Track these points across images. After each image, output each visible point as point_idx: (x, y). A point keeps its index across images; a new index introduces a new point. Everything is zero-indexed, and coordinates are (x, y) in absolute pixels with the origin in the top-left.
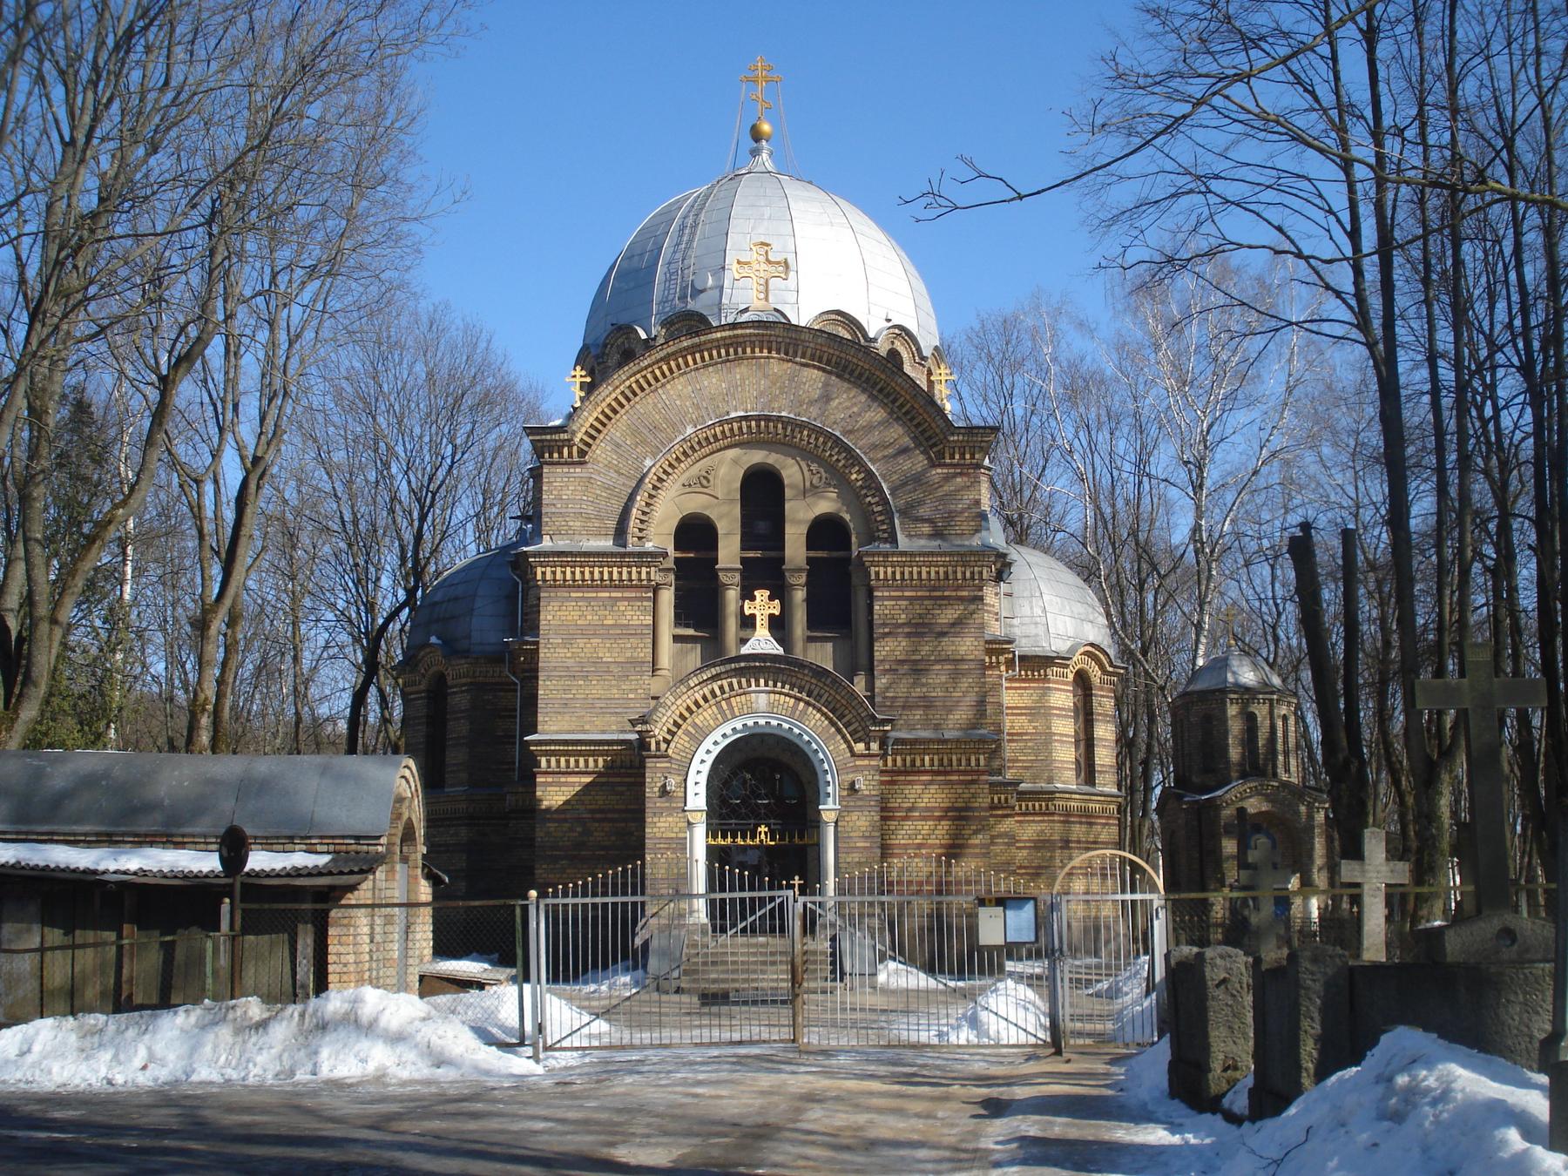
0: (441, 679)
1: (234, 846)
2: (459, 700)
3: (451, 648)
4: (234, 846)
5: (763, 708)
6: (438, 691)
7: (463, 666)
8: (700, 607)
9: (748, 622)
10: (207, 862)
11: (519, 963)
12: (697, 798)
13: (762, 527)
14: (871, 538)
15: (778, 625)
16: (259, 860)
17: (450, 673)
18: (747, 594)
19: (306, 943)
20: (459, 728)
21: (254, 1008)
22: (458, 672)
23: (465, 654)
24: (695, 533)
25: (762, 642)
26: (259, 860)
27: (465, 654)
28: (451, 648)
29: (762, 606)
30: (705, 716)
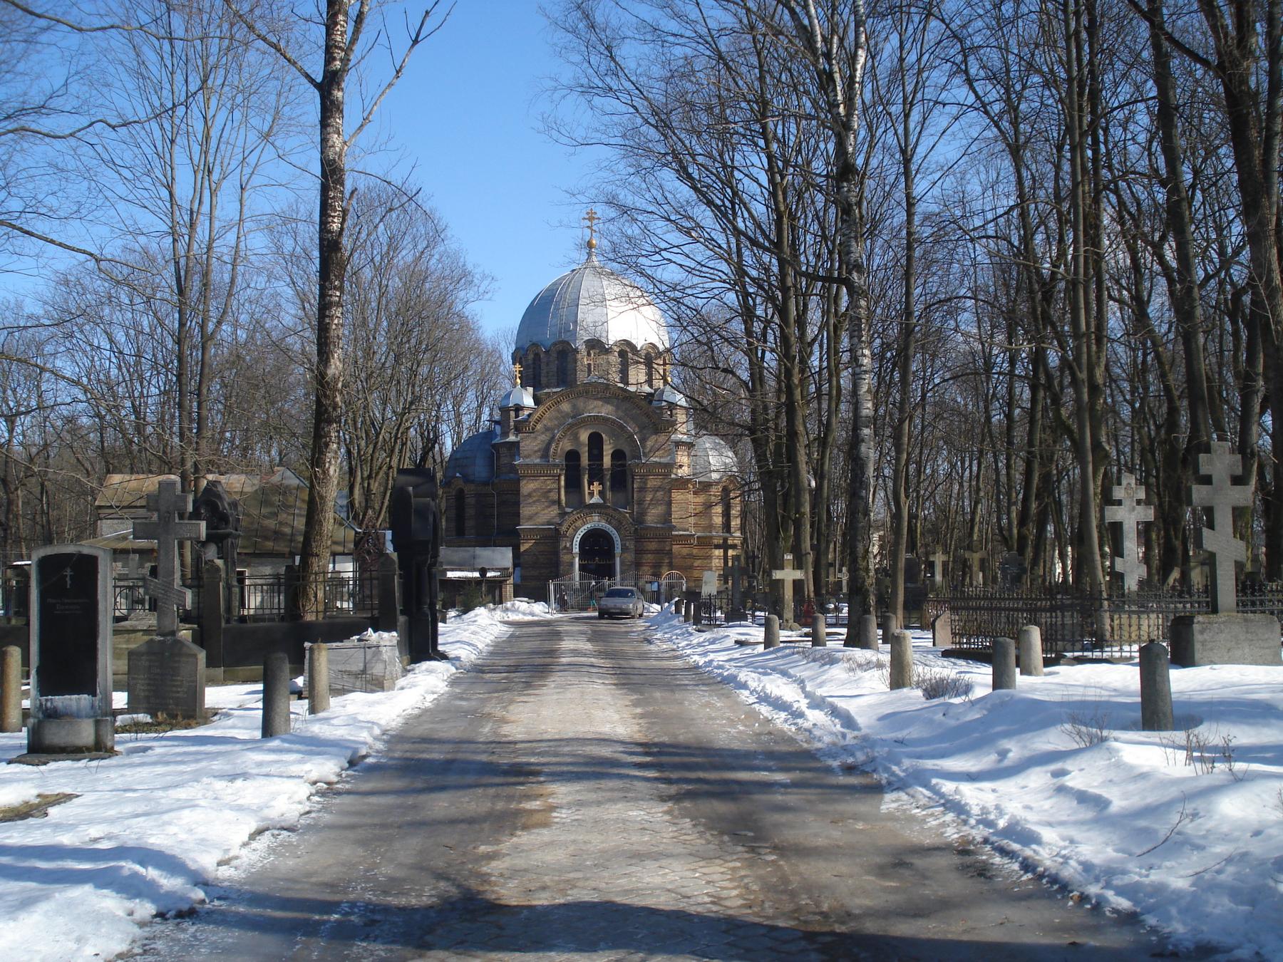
0: (461, 491)
1: (483, 572)
2: (470, 500)
3: (466, 479)
4: (483, 572)
5: (596, 521)
6: (460, 496)
7: (472, 487)
8: (574, 485)
9: (592, 494)
10: (477, 574)
11: (306, 673)
12: (576, 550)
13: (595, 452)
14: (634, 458)
15: (601, 493)
16: (489, 575)
17: (466, 489)
18: (590, 483)
19: (497, 592)
20: (470, 512)
21: (491, 605)
22: (469, 489)
23: (473, 482)
24: (573, 456)
25: (596, 499)
26: (489, 575)
27: (473, 482)
28: (466, 479)
29: (596, 487)
30: (579, 523)
